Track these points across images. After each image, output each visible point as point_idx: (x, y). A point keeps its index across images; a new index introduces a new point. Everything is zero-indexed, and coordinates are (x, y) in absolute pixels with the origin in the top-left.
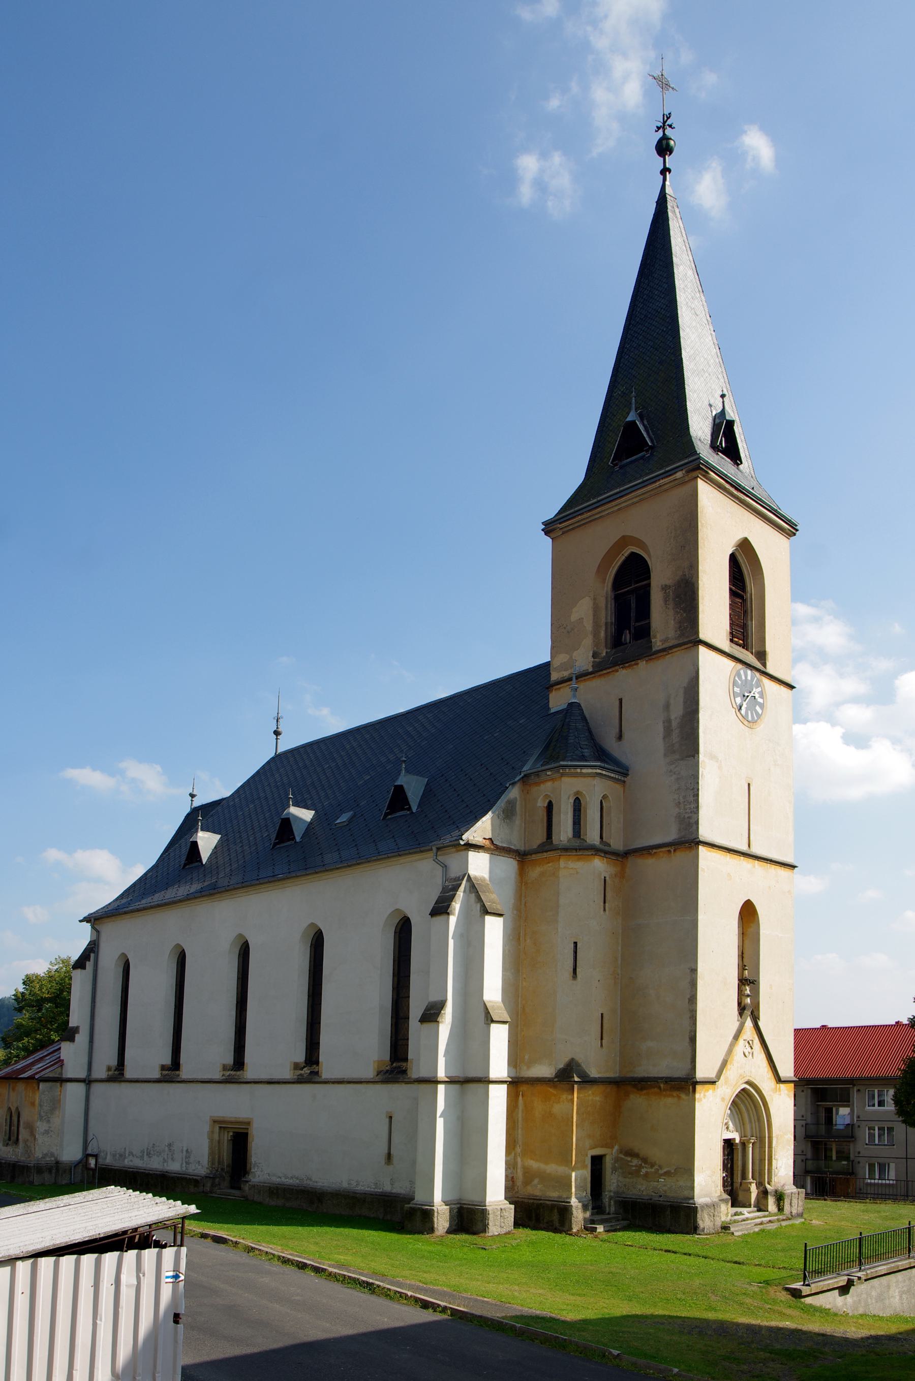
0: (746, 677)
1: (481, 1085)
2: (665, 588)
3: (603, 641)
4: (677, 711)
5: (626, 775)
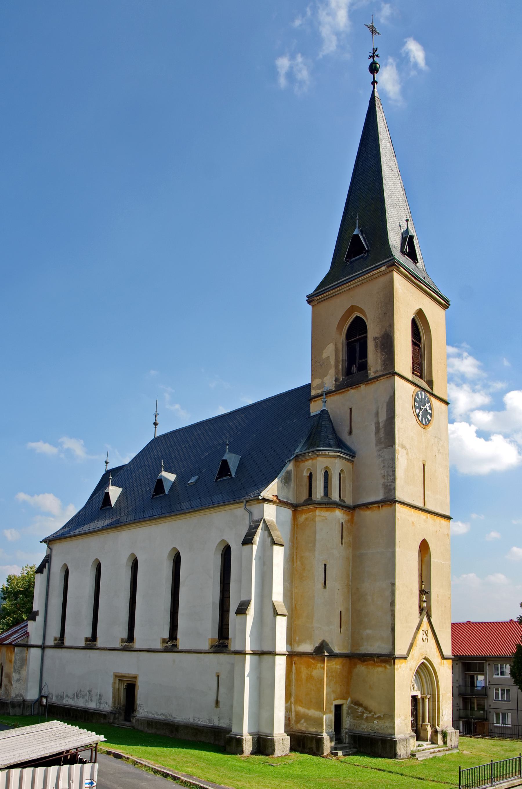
2: (375, 339)
4: (383, 418)
5: (354, 457)
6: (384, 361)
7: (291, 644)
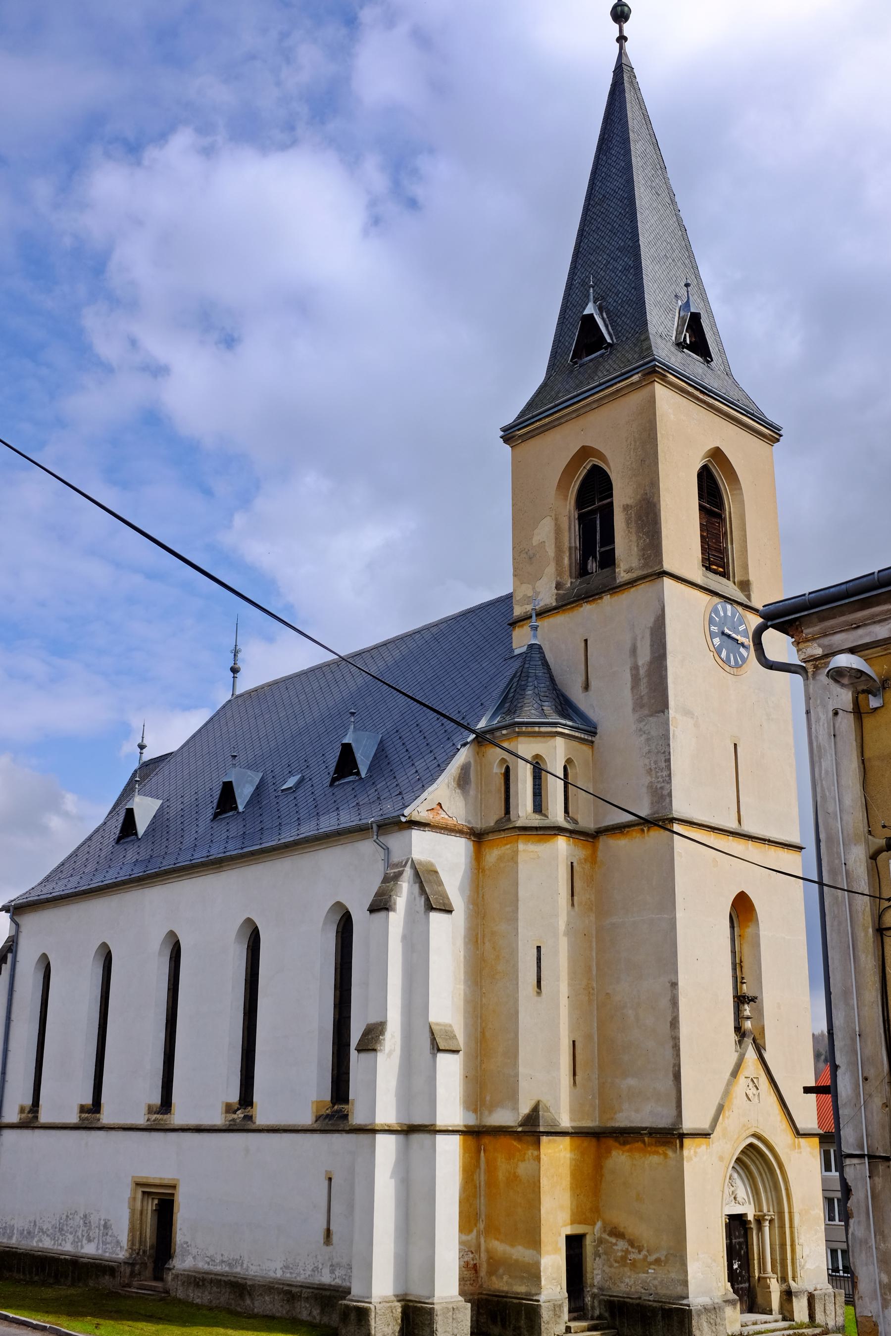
0: (725, 611)
1: (363, 1138)
2: (626, 508)
3: (567, 568)
4: (644, 656)
5: (594, 734)
6: (643, 549)
7: (475, 1111)
